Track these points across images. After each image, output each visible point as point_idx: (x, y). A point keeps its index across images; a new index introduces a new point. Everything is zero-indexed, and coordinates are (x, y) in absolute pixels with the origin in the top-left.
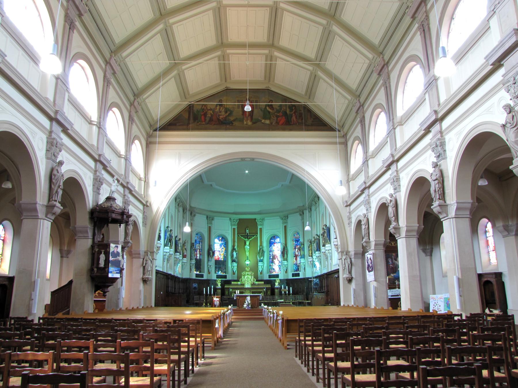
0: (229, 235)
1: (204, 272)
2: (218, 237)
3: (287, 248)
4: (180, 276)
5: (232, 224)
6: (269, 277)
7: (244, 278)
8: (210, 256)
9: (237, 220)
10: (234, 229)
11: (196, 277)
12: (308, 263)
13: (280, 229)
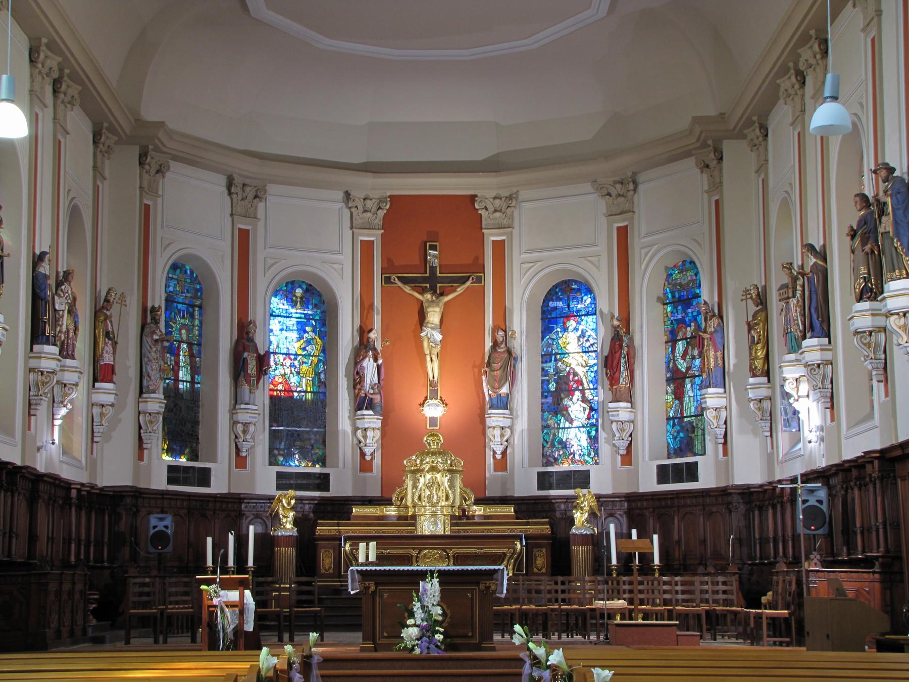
0: (342, 274)
1: (214, 460)
2: (287, 290)
3: (631, 340)
4: (67, 473)
5: (358, 221)
6: (541, 486)
7: (415, 486)
8: (242, 379)
9: (382, 200)
10: (367, 247)
11: (170, 481)
12: (744, 412)
13: (594, 245)
